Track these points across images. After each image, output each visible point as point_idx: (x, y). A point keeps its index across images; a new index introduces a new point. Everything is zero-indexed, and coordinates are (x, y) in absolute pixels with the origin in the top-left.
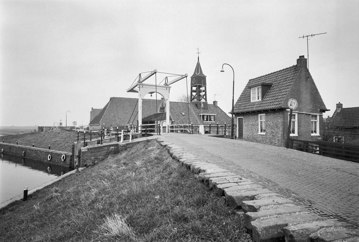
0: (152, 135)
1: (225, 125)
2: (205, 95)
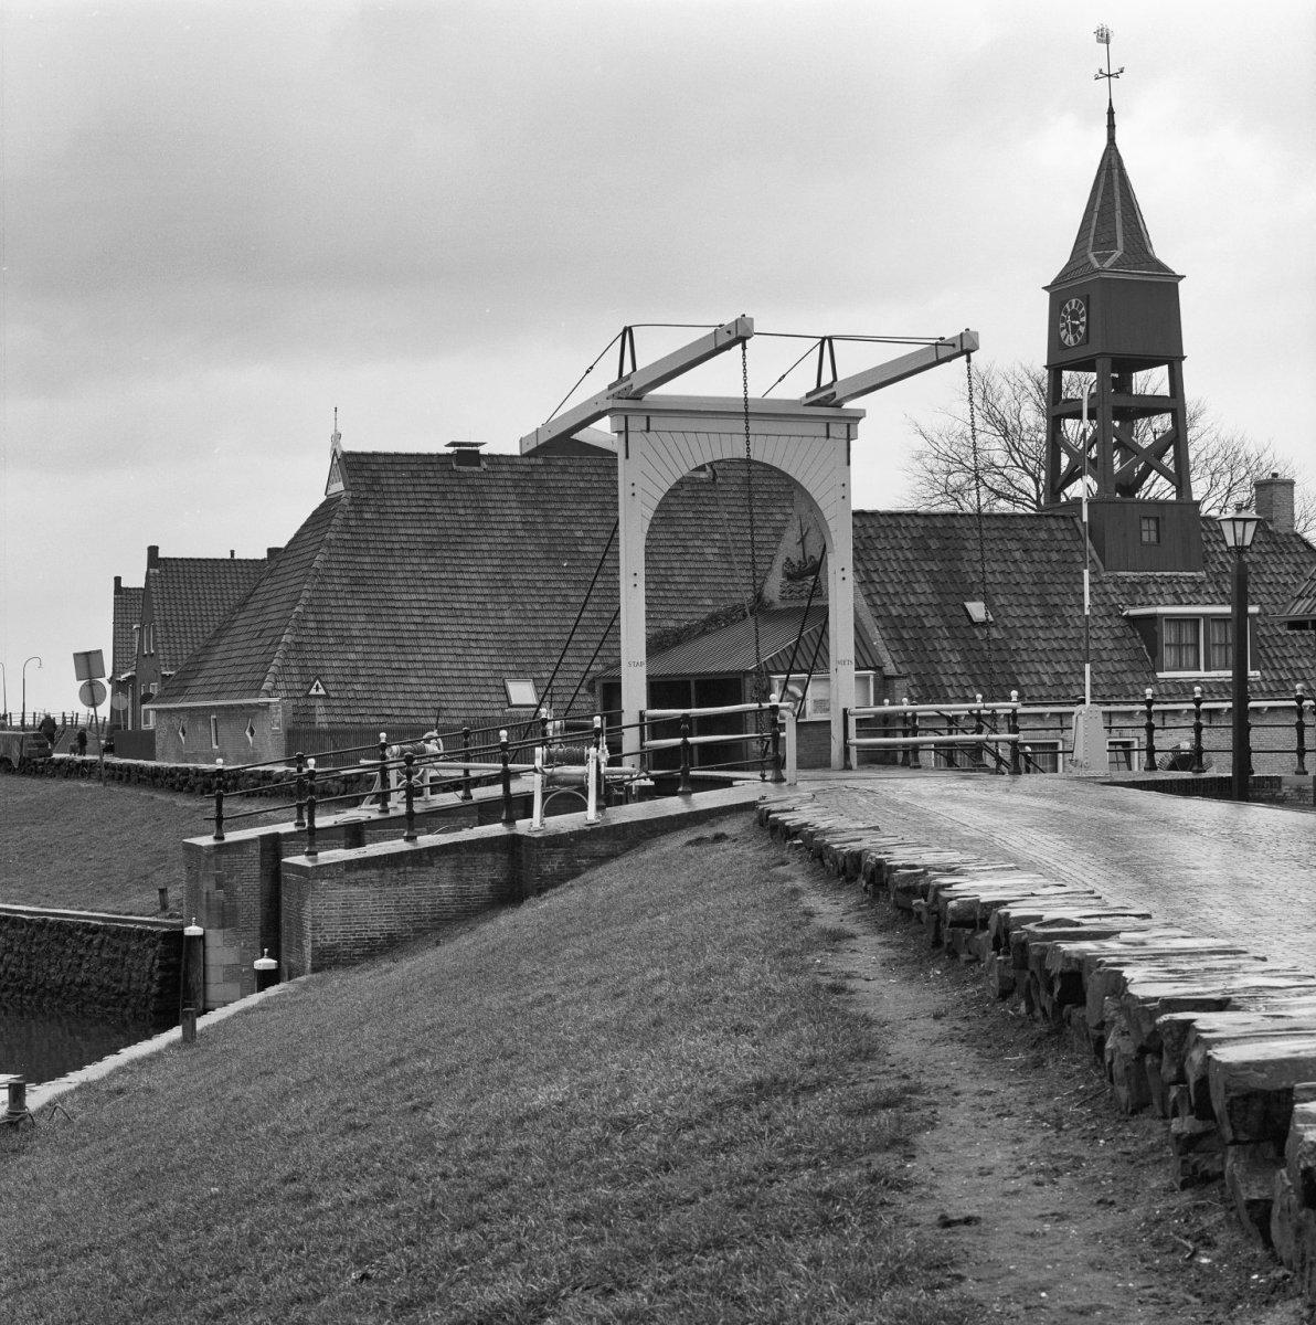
0: (727, 783)
1: (1149, 703)
2: (1177, 437)
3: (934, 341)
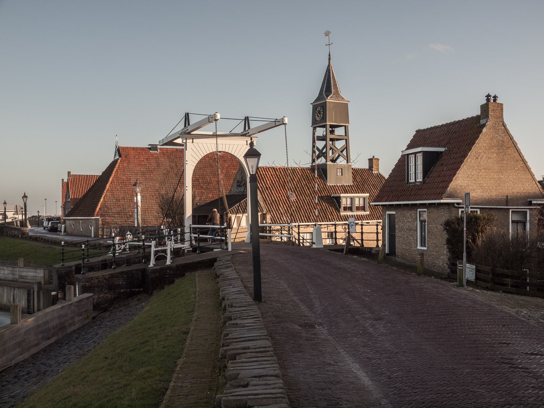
3: (274, 120)
